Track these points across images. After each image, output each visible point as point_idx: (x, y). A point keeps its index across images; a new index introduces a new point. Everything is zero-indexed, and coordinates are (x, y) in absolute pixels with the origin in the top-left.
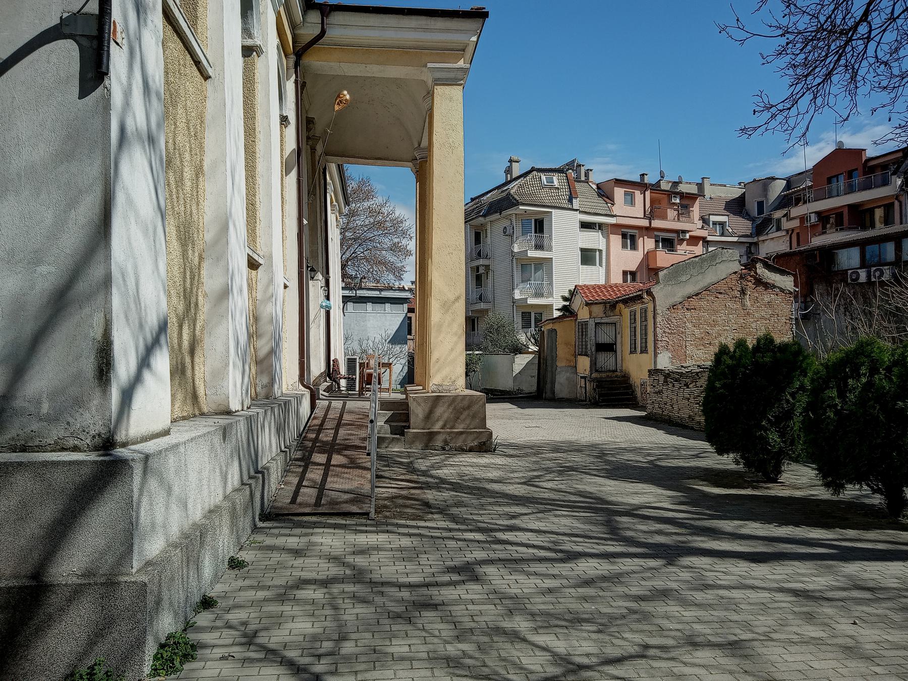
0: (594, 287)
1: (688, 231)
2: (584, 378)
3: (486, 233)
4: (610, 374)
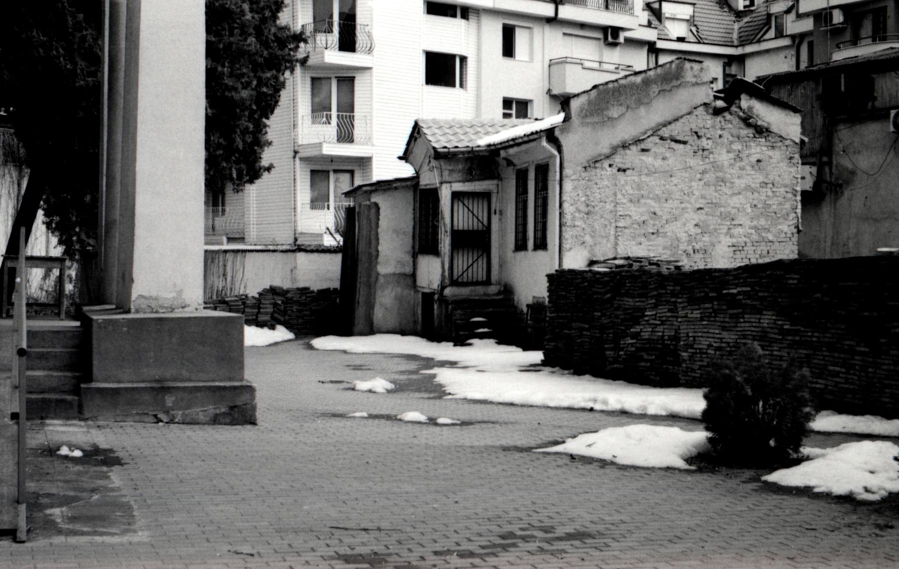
1: (622, 29)
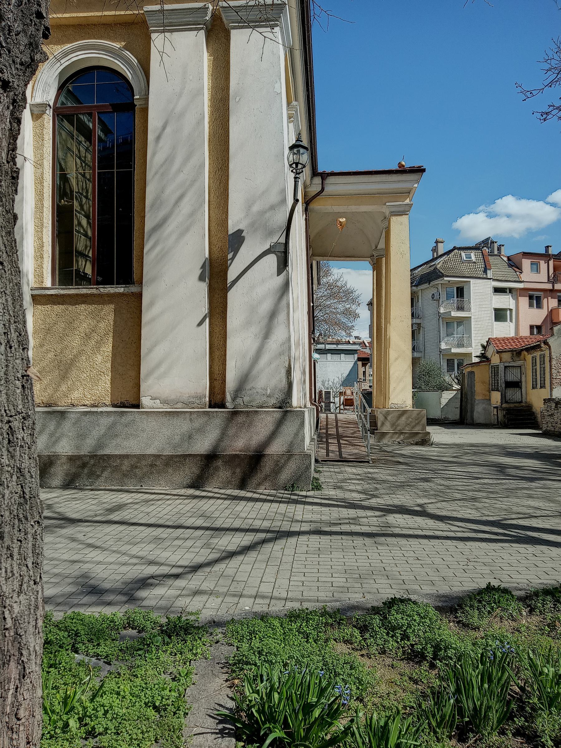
0: (503, 339)
2: (497, 408)
3: (418, 298)
4: (517, 405)
